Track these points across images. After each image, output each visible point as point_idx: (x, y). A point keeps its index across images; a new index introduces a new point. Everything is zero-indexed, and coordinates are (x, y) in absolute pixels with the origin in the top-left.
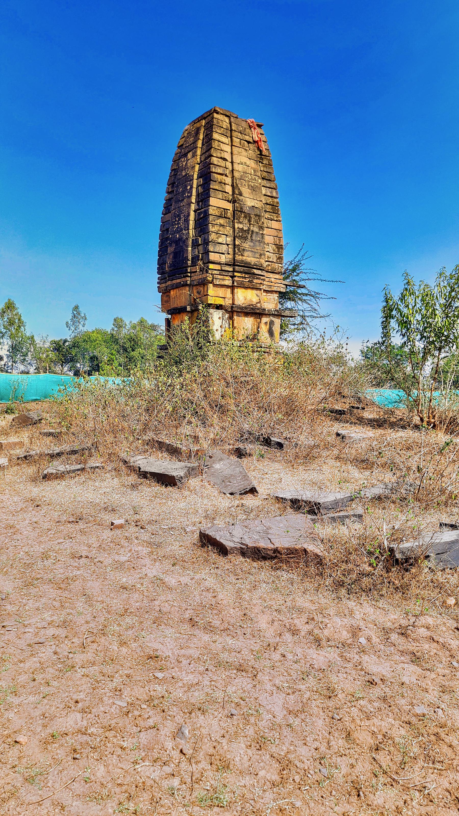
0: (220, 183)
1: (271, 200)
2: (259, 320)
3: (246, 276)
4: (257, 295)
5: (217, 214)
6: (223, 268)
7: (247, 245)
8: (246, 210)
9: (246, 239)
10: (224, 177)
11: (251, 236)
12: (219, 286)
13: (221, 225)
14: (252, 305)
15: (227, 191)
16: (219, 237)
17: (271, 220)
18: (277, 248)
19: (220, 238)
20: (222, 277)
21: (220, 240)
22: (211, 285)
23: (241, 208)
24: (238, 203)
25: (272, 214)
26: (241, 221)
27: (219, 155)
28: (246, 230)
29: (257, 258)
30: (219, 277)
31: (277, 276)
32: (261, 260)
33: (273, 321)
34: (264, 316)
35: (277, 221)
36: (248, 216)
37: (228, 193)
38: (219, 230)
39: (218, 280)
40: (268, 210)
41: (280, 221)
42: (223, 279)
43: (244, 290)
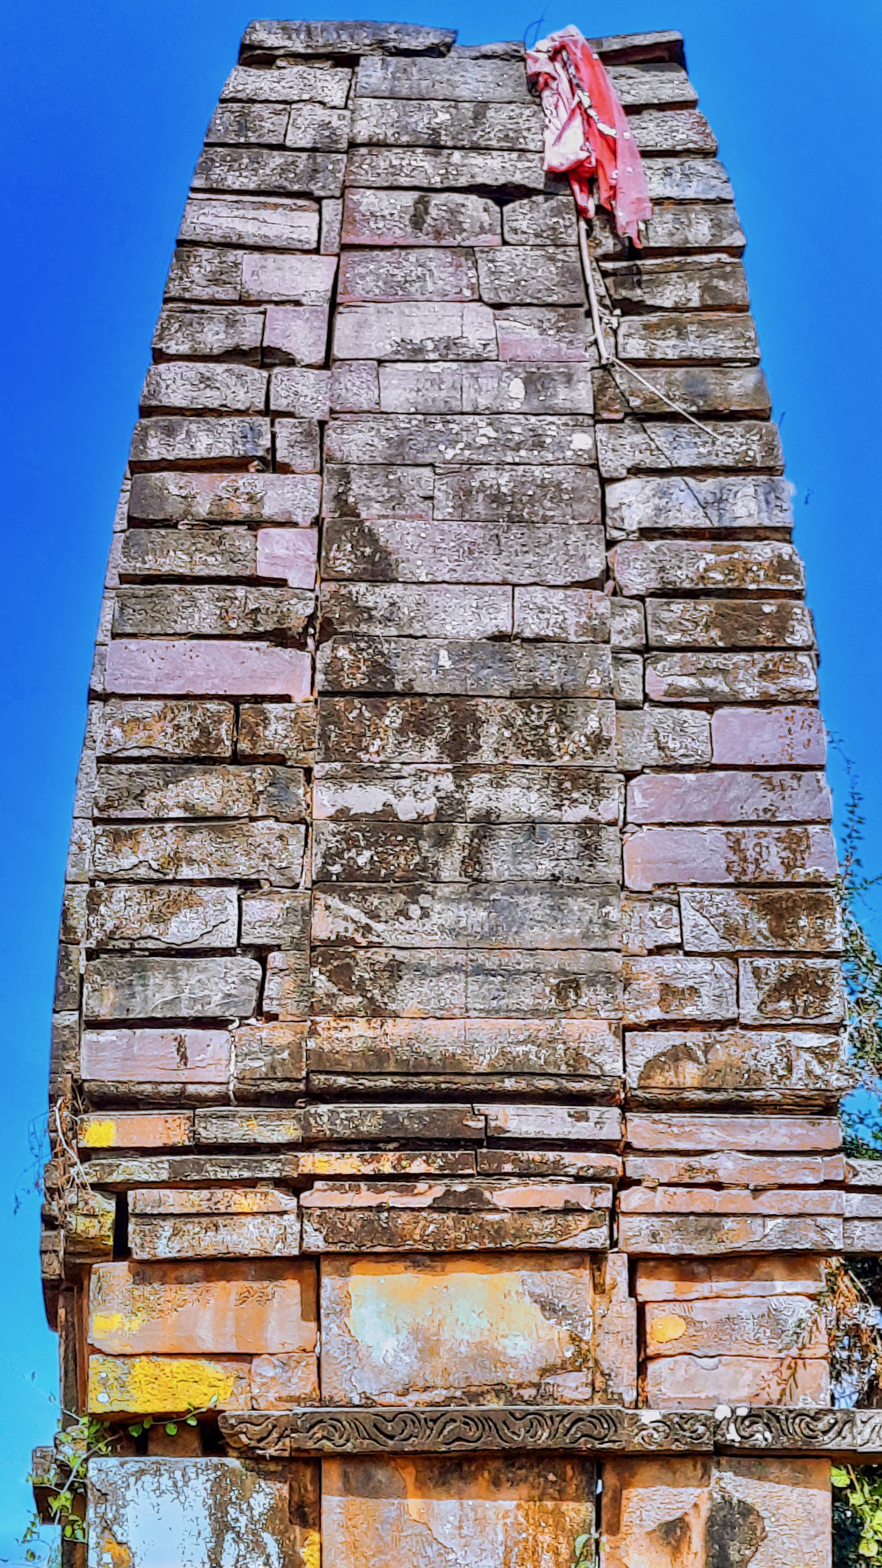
3: (418, 1166)
4: (548, 1307)
8: (417, 669)
9: (415, 883)
11: (473, 859)
12: (185, 1272)
13: (195, 819)
14: (500, 1390)
15: (263, 571)
16: (175, 905)
17: (710, 708)
18: (767, 907)
19: (186, 914)
20: (196, 1200)
21: (182, 929)
23: (380, 668)
25: (716, 660)
29: (535, 1013)
30: (175, 1200)
31: (779, 1132)
33: (746, 1510)
34: (648, 1471)
35: (765, 702)
36: (451, 725)
37: (280, 583)
39: (167, 1228)
40: (672, 639)
42: (212, 1216)
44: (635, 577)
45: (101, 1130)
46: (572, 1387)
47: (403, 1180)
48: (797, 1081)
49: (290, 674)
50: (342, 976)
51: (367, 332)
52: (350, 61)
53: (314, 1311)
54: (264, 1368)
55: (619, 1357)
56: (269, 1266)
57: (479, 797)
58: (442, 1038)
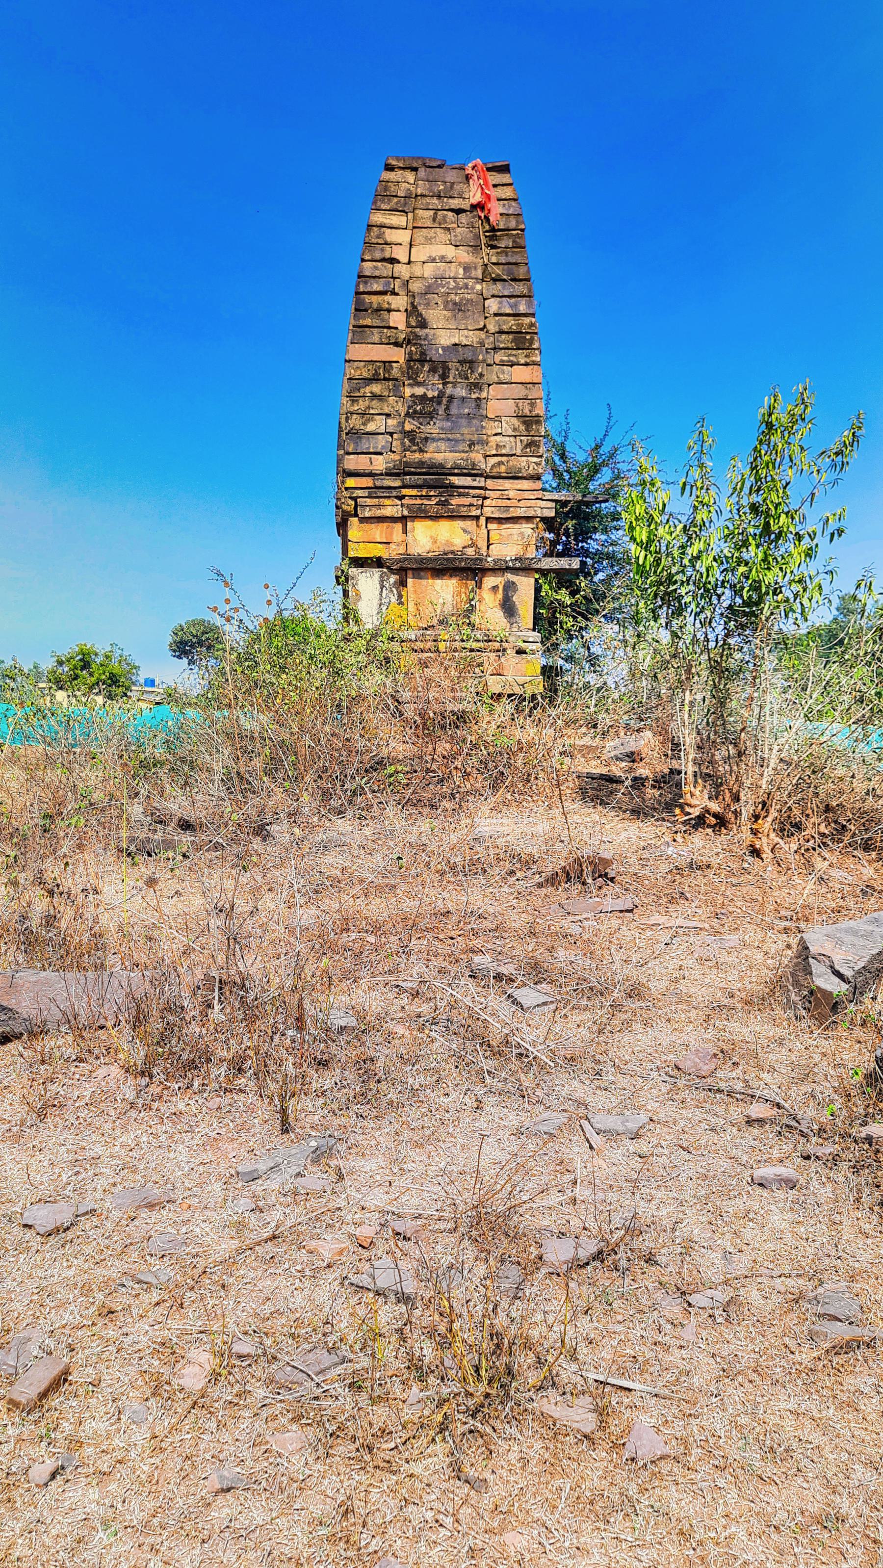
0: (378, 310)
1: (513, 322)
2: (471, 584)
3: (432, 493)
4: (465, 531)
5: (365, 375)
6: (378, 483)
7: (433, 429)
9: (431, 416)
10: (388, 298)
11: (447, 408)
12: (372, 520)
13: (374, 396)
14: (452, 552)
15: (392, 325)
16: (368, 420)
17: (511, 366)
18: (524, 423)
19: (371, 423)
20: (375, 501)
21: (371, 427)
22: (354, 520)
23: (423, 353)
24: (415, 344)
25: (514, 352)
26: (420, 379)
27: (378, 255)
28: (434, 397)
29: (463, 452)
30: (369, 501)
32: (473, 455)
33: (513, 583)
34: (490, 573)
35: (526, 364)
36: (441, 369)
37: (396, 328)
38: (369, 408)
39: (368, 508)
40: (502, 346)
41: (535, 363)
42: (379, 506)
43: (429, 523)
44: (492, 328)
45: (351, 482)
46: (470, 552)
47: (428, 497)
48: (531, 471)
49: (398, 355)
50: (412, 441)
51: (420, 253)
52: (415, 169)
53: (405, 531)
54: (392, 546)
55: (482, 544)
56: (393, 519)
57: (449, 391)
58: (439, 458)
